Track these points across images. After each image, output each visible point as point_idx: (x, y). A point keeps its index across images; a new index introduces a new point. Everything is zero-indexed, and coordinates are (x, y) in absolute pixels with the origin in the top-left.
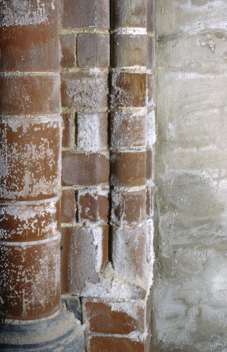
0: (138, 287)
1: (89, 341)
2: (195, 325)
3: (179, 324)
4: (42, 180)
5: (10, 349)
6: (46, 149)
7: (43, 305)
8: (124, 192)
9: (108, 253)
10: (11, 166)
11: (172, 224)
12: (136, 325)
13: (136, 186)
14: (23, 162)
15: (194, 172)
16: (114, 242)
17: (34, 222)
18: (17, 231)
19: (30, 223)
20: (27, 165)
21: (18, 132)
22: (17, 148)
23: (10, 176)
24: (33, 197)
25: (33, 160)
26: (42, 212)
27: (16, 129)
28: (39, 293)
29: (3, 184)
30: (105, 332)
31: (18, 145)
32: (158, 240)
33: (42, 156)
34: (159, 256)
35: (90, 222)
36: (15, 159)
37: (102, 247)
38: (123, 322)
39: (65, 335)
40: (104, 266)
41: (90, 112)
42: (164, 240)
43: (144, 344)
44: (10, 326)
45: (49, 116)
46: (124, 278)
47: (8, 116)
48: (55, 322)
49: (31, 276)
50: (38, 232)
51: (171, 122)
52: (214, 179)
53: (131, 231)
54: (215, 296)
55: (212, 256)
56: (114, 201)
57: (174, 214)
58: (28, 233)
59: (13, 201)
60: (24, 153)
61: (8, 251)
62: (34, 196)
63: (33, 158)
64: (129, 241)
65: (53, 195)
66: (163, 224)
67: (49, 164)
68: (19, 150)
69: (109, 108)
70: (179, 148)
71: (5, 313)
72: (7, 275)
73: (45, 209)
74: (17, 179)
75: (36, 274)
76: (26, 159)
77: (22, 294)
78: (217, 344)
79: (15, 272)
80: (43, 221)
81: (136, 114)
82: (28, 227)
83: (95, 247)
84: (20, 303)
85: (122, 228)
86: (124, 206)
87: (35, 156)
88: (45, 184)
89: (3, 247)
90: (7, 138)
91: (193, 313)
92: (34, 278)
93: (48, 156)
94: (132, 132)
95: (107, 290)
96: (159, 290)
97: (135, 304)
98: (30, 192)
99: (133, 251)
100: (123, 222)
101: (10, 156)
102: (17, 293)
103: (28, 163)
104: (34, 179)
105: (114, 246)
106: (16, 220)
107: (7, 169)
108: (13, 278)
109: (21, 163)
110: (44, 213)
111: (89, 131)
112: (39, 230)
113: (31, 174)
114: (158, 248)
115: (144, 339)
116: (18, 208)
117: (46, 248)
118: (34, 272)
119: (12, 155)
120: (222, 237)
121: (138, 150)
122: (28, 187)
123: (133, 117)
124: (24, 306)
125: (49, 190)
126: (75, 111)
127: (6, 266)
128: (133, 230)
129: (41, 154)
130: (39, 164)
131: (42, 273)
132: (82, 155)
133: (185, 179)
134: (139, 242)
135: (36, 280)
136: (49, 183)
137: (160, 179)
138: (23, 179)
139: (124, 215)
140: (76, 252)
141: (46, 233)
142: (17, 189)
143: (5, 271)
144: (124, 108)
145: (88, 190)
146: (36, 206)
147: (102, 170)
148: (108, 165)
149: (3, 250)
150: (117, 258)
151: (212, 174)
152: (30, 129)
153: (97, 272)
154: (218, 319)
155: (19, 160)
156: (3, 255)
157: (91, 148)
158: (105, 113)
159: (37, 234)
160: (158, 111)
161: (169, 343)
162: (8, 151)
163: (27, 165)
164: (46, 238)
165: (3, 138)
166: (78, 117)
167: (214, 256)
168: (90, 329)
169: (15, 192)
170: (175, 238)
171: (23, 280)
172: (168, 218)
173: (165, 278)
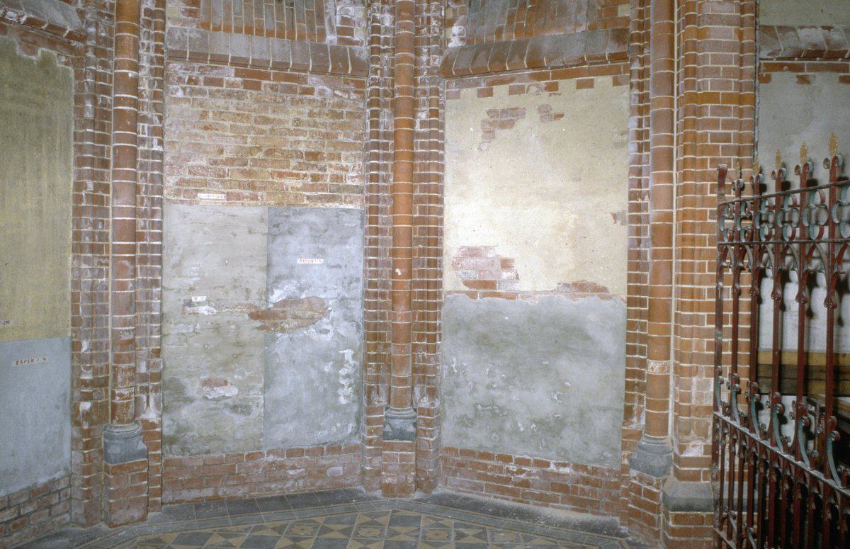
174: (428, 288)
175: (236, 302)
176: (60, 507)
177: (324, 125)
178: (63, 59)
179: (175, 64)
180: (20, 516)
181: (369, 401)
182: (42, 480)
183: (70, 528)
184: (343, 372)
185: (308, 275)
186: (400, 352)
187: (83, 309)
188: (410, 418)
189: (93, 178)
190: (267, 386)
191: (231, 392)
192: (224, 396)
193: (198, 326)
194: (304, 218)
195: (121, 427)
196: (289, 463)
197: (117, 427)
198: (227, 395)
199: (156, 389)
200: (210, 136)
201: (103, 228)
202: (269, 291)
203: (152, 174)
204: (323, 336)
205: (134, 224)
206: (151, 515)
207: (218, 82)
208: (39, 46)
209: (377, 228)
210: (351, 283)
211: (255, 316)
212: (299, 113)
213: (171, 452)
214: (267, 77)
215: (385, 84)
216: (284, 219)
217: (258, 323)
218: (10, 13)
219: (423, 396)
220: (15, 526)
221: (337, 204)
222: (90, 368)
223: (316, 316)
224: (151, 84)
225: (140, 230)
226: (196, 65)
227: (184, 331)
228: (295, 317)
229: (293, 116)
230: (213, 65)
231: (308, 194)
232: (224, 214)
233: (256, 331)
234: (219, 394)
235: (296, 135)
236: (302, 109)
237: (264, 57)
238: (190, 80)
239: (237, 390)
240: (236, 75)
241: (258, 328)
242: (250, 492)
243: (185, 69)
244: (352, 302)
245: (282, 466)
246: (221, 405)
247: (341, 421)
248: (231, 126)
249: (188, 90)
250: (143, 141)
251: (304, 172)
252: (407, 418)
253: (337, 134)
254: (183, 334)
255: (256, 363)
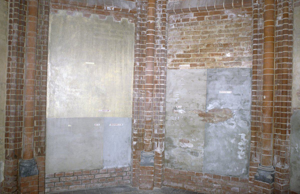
39: (174, 69)
40: (157, 147)
65: (151, 138)
174: (282, 106)
175: (194, 109)
176: (127, 177)
177: (232, 31)
178: (131, 21)
179: (171, 16)
180: (111, 177)
181: (251, 160)
182: (120, 166)
183: (129, 186)
184: (240, 144)
185: (224, 98)
186: (265, 138)
187: (135, 108)
188: (269, 172)
189: (139, 61)
190: (205, 146)
191: (191, 146)
192: (188, 147)
193: (178, 118)
194: (223, 73)
195: (145, 153)
196: (214, 181)
197: (144, 153)
198: (189, 147)
199: (161, 140)
200: (184, 42)
201: (142, 79)
202: (207, 105)
203: (161, 58)
204: (231, 126)
205: (153, 77)
206: (155, 188)
207: (187, 20)
208: (122, 17)
209: (257, 76)
210: (245, 102)
211: (201, 115)
212: (221, 27)
213: (167, 166)
214: (207, 14)
215: (260, 6)
216: (214, 73)
217: (202, 118)
218: (108, 8)
219: (278, 162)
220: (109, 180)
221: (238, 66)
222: (136, 129)
223: (228, 117)
224: (161, 25)
225: (156, 80)
226: (179, 15)
227: (173, 119)
228: (218, 117)
229: (218, 29)
230: (185, 13)
231: (225, 62)
232: (189, 72)
233: (201, 121)
234: (186, 146)
235: (220, 37)
236: (222, 25)
237: (203, 6)
238: (177, 21)
239: (193, 145)
240: (194, 16)
241: (202, 120)
242: (197, 189)
243: (175, 17)
244: (245, 112)
245: (210, 182)
246: (186, 151)
247: (239, 167)
248: (192, 37)
249: (176, 25)
250: (157, 46)
251: (223, 53)
252: (267, 171)
253: (239, 34)
254: (173, 120)
255: (201, 135)
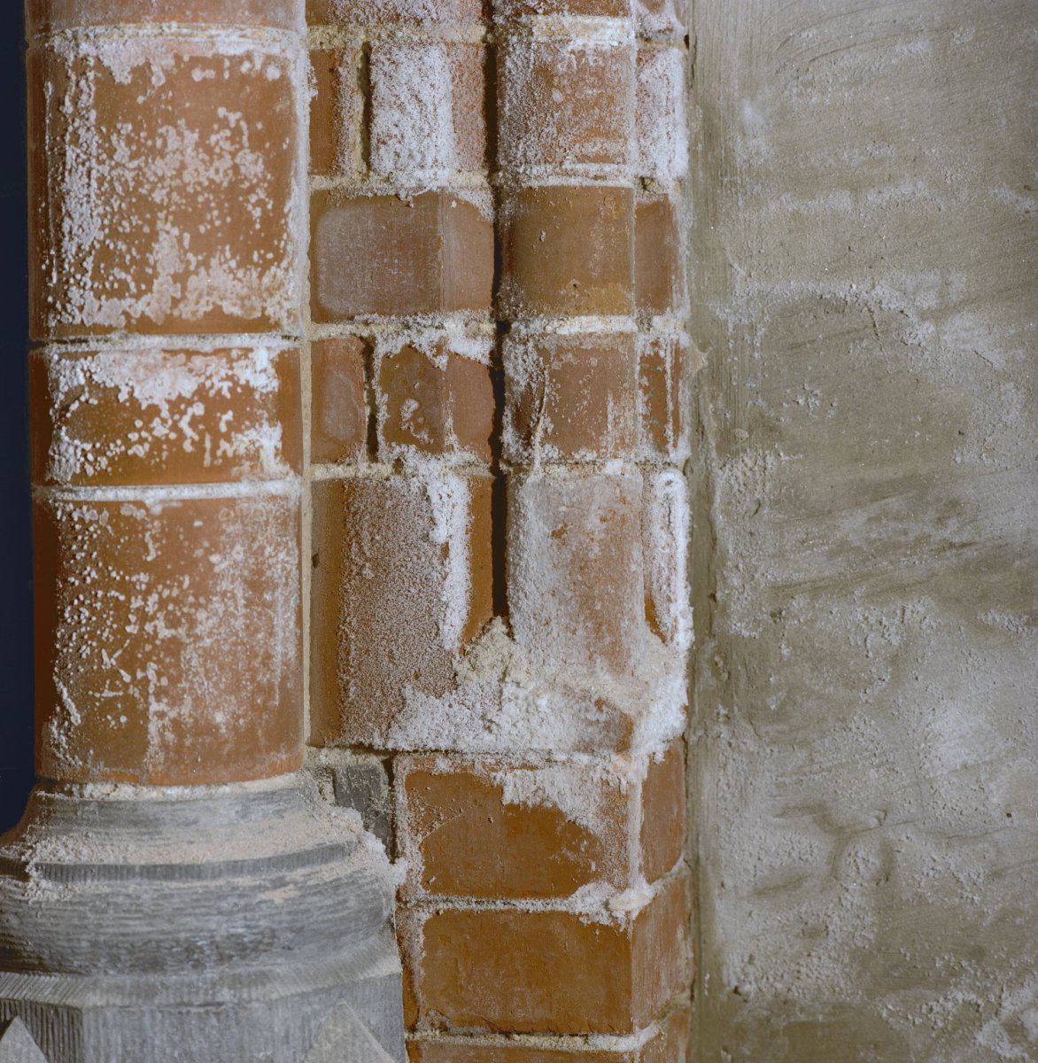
0: (599, 704)
1: (420, 931)
2: (869, 919)
3: (806, 912)
4: (223, 260)
5: (96, 882)
6: (237, 151)
7: (223, 730)
8: (543, 335)
9: (491, 584)
10: (108, 208)
11: (766, 499)
12: (597, 857)
13: (590, 312)
14: (151, 191)
15: (843, 289)
16: (511, 535)
17: (190, 411)
18: (128, 444)
19: (177, 417)
20: (165, 204)
21: (134, 82)
22: (129, 141)
23: (107, 242)
24: (187, 321)
25: (189, 184)
26: (222, 380)
27: (126, 73)
28: (211, 684)
29: (83, 275)
30: (482, 892)
31: (133, 130)
32: (713, 567)
33: (221, 174)
34: (715, 628)
35: (419, 455)
36: (123, 179)
37: (466, 554)
38: (549, 847)
41: (416, 38)
42: (737, 567)
43: (630, 936)
44: (103, 805)
45: (249, 31)
46: (550, 670)
47: (100, 30)
48: (269, 806)
49: (179, 614)
50: (204, 450)
51: (753, 97)
52: (924, 316)
53: (572, 487)
54: (942, 790)
55: (924, 627)
56: (512, 374)
57: (770, 459)
58: (169, 450)
59: (114, 336)
60: (154, 160)
61: (97, 522)
62: (189, 315)
63: (187, 177)
64: (566, 525)
66: (730, 503)
67: (250, 207)
68: (139, 148)
69: (491, 28)
70: (783, 198)
71: (86, 762)
72: (93, 610)
73: (231, 368)
74: (131, 254)
75: (196, 609)
76: (162, 179)
77: (146, 680)
78: (960, 997)
79: (122, 598)
80: (225, 412)
81: (586, 41)
82: (166, 431)
83: (438, 552)
84: (139, 717)
85: (541, 475)
86: (547, 390)
87: (196, 170)
88: (231, 276)
89: (81, 508)
90: (95, 106)
91: (862, 867)
92: (192, 623)
93: (246, 178)
94: (570, 106)
95: (483, 717)
96: (721, 773)
97: (591, 774)
98: (175, 302)
99: (580, 564)
100: (539, 452)
101: (105, 169)
102: (127, 678)
103: (168, 194)
104: (190, 256)
105: (511, 551)
106: (128, 404)
107: (95, 218)
108: (113, 623)
109: (145, 195)
110: (230, 384)
111: (412, 107)
112: (208, 445)
113: (181, 235)
114: (713, 597)
115: (628, 913)
116: (133, 360)
117: (236, 516)
118: (191, 599)
119: (112, 168)
120: (964, 545)
121: (596, 178)
122: (171, 281)
123: (573, 52)
124: (153, 728)
125: (246, 302)
126: (362, 38)
127: (89, 580)
128: (580, 482)
129: (216, 164)
130: (207, 201)
131: (220, 608)
132: (388, 203)
133: (812, 317)
134: (607, 531)
135: (198, 631)
136: (248, 276)
137: (715, 320)
138: (151, 253)
139: (544, 424)
140: (368, 573)
141: (236, 460)
142: (128, 289)
143: (85, 598)
144: (540, 18)
145: (413, 333)
146: (197, 353)
147: (464, 258)
148: (488, 240)
149: (79, 518)
150: (521, 595)
151: (914, 294)
152: (175, 71)
153: (447, 648)
154: (962, 888)
155: (139, 184)
156: (80, 538)
157: (419, 174)
158: (477, 47)
159: (203, 459)
160: (699, 58)
161: (769, 997)
162: (99, 154)
163: (165, 204)
164: (237, 479)
165: (83, 109)
166: (373, 57)
167: (934, 624)
168: (426, 883)
169: (123, 302)
170: (780, 555)
171: (149, 627)
172: (749, 474)
173: (744, 723)
